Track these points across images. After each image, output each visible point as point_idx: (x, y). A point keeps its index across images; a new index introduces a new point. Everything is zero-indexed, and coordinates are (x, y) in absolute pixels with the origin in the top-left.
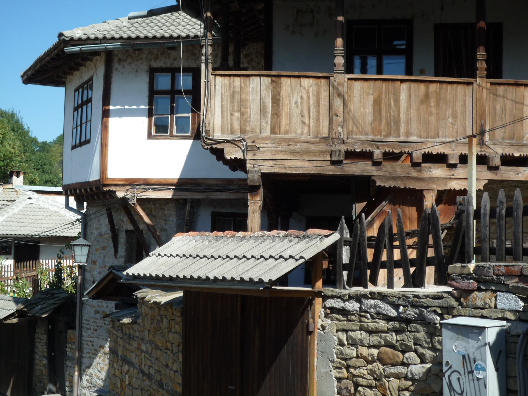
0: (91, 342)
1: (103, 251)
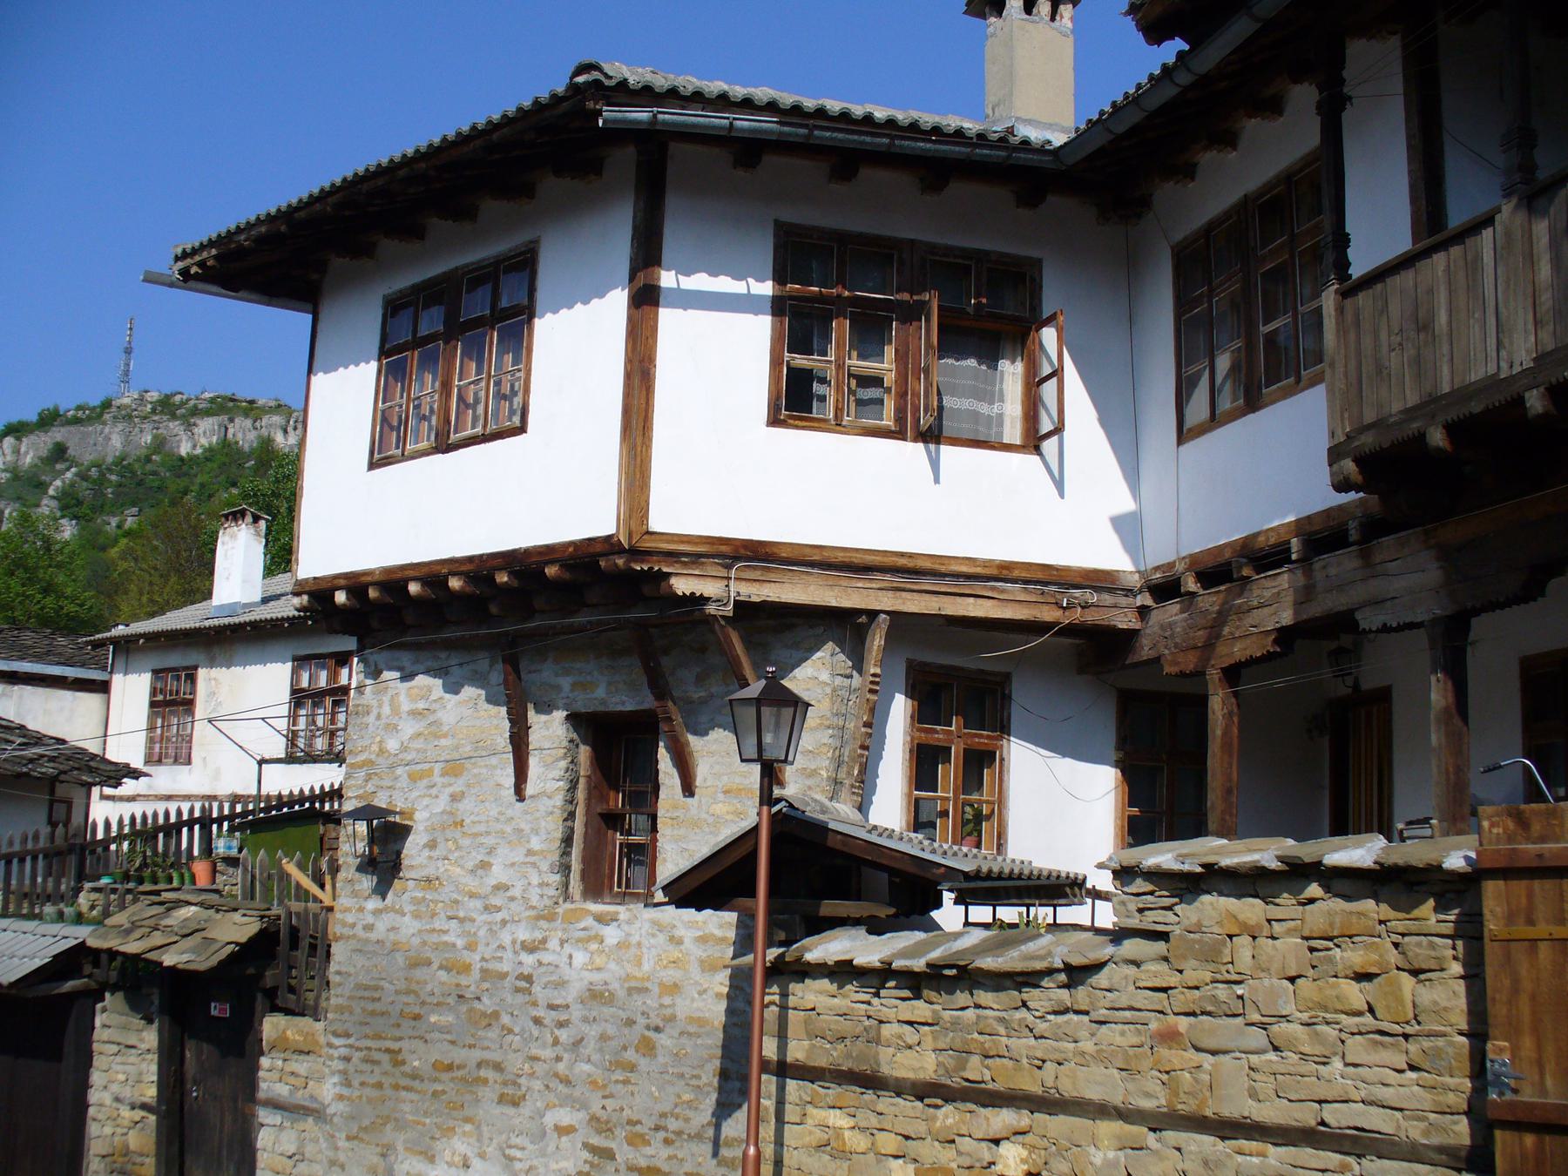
0: (388, 1051)
1: (446, 780)
